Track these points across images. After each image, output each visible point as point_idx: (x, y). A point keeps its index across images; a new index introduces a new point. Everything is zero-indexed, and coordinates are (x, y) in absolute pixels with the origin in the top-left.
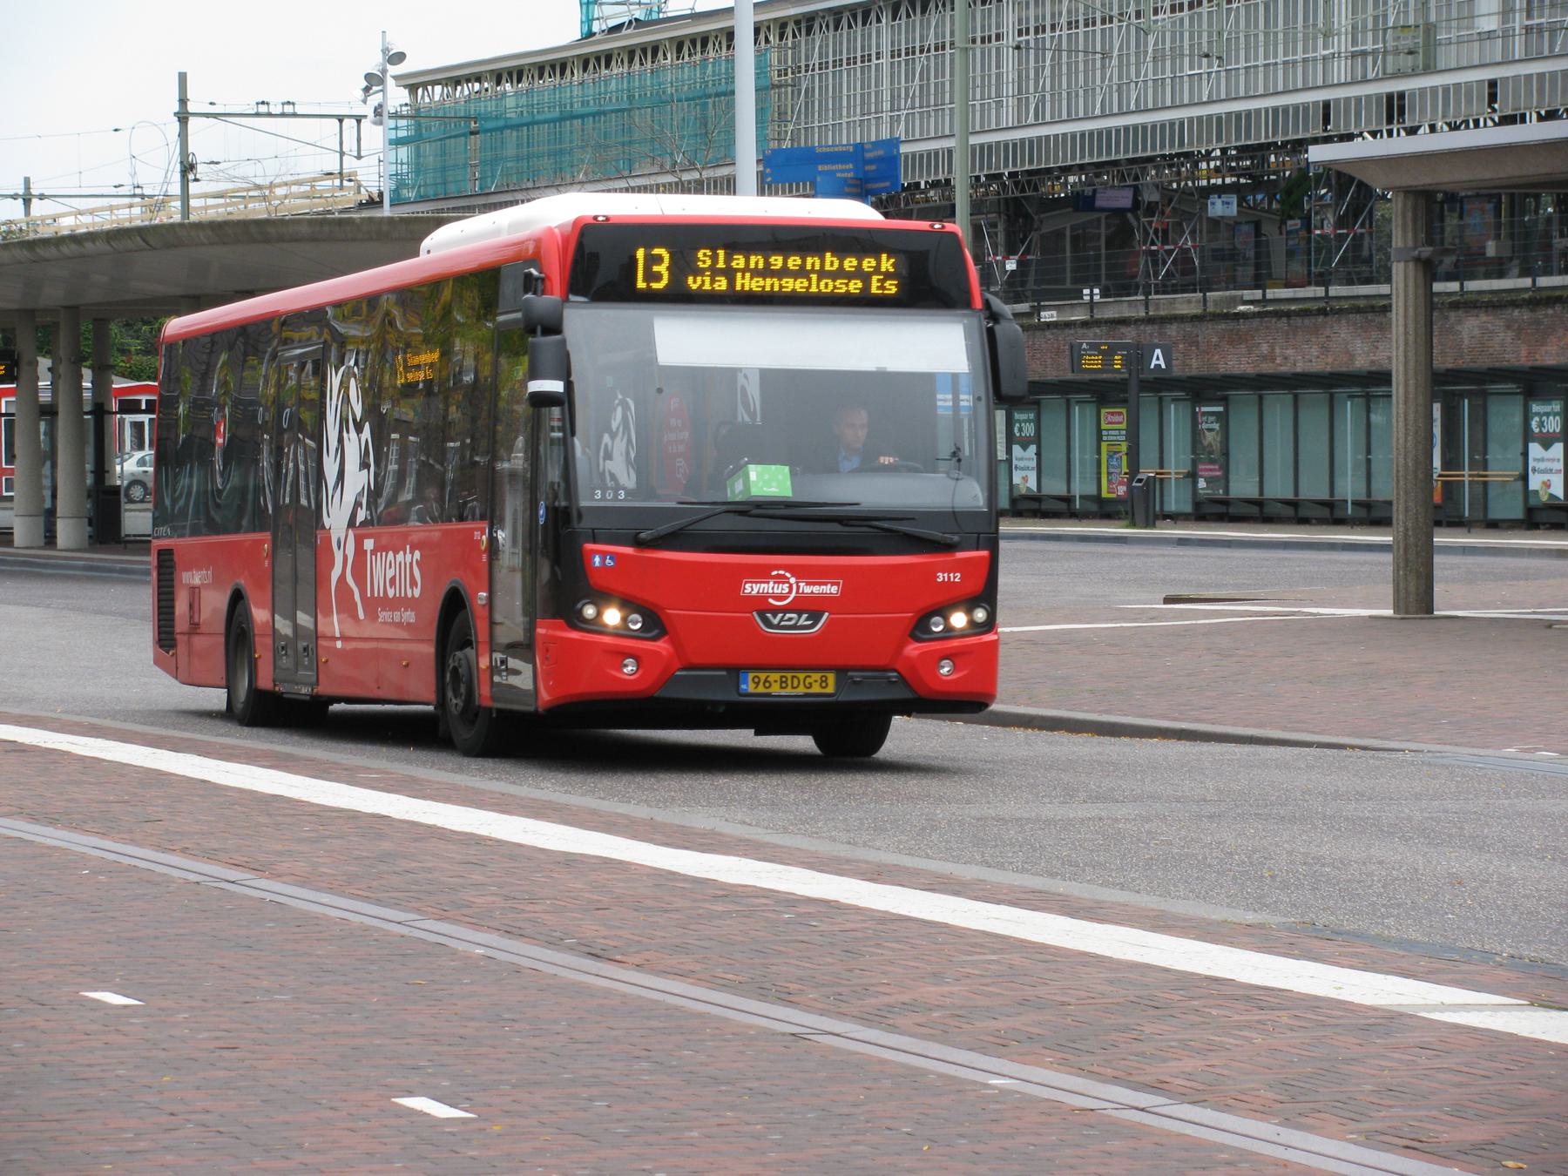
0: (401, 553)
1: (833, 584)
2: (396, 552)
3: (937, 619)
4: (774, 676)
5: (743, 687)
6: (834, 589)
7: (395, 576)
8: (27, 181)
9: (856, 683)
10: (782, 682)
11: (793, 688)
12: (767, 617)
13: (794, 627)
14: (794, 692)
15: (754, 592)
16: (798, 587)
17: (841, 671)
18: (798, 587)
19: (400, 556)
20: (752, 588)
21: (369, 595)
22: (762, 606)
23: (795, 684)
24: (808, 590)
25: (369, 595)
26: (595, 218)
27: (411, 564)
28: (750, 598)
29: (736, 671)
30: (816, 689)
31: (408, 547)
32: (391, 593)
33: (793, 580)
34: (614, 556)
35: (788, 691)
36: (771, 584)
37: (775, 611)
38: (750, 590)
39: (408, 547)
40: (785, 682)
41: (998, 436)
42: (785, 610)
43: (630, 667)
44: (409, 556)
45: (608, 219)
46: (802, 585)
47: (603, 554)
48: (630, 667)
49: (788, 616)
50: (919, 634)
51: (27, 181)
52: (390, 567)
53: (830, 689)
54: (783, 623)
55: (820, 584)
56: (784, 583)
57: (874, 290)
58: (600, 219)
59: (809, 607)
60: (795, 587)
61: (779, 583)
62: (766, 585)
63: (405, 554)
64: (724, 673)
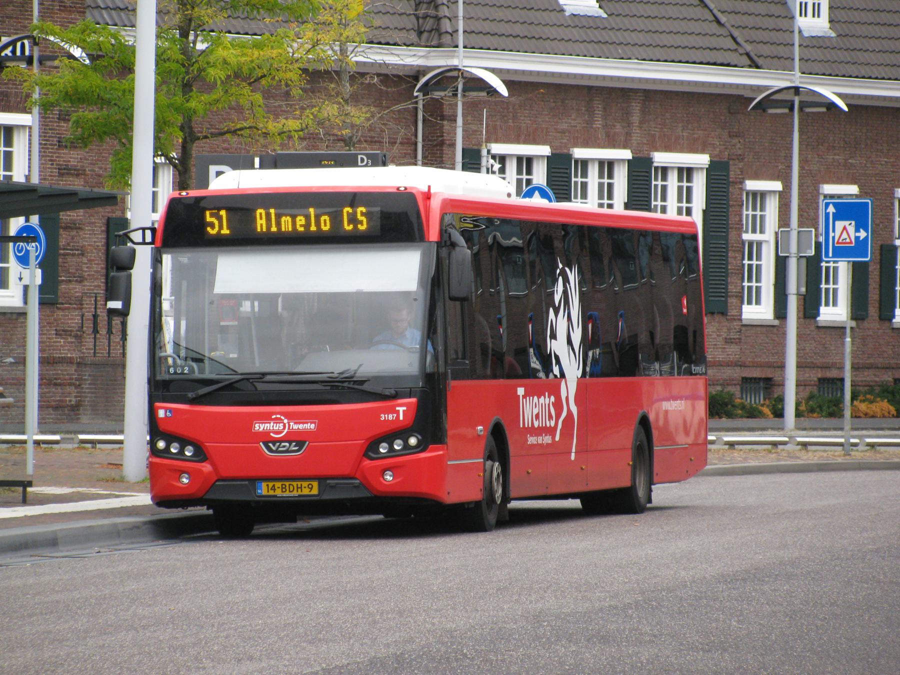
0: (543, 397)
1: (311, 423)
2: (539, 397)
3: (384, 445)
4: (278, 484)
5: (259, 491)
6: (313, 426)
7: (539, 413)
8: (429, 187)
9: (355, 487)
10: (282, 488)
11: (290, 491)
12: (269, 446)
13: (287, 451)
14: (292, 494)
15: (261, 429)
16: (289, 426)
17: (321, 479)
18: (289, 426)
19: (542, 399)
20: (259, 427)
21: (521, 426)
22: (266, 438)
23: (291, 489)
24: (296, 427)
25: (521, 426)
26: (398, 189)
27: (549, 405)
28: (259, 433)
29: (254, 480)
30: (306, 492)
31: (547, 394)
32: (536, 424)
33: (286, 421)
34: (171, 410)
35: (287, 494)
36: (272, 424)
37: (274, 441)
38: (258, 428)
39: (547, 394)
40: (285, 488)
41: (871, 288)
42: (281, 441)
43: (389, 477)
44: (547, 399)
45: (406, 188)
46: (291, 424)
47: (166, 409)
48: (389, 477)
49: (283, 444)
50: (371, 454)
51: (429, 187)
52: (536, 407)
53: (315, 491)
54: (280, 449)
55: (303, 423)
56: (280, 423)
57: (283, 229)
58: (402, 189)
59: (298, 439)
60: (287, 425)
61: (277, 423)
62: (268, 425)
63: (545, 398)
64: (247, 483)
